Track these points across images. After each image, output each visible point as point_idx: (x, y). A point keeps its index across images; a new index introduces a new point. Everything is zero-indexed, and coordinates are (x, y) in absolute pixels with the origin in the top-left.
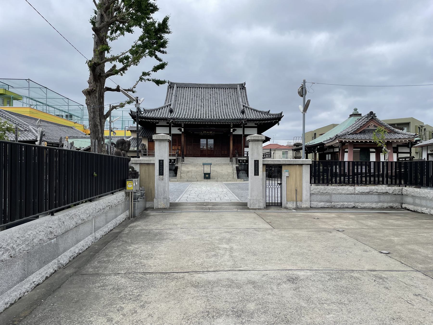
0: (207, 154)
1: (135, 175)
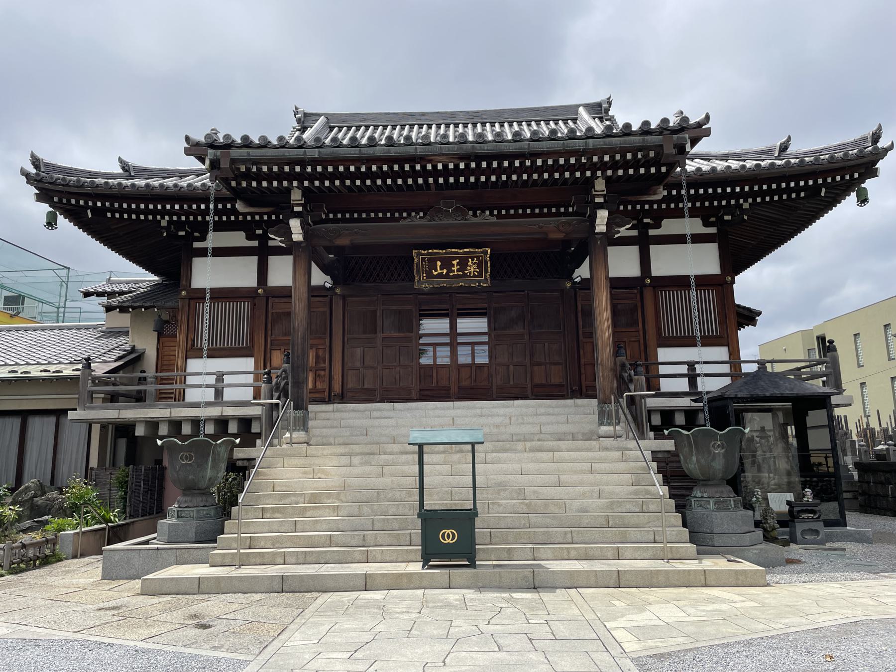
0: (454, 389)
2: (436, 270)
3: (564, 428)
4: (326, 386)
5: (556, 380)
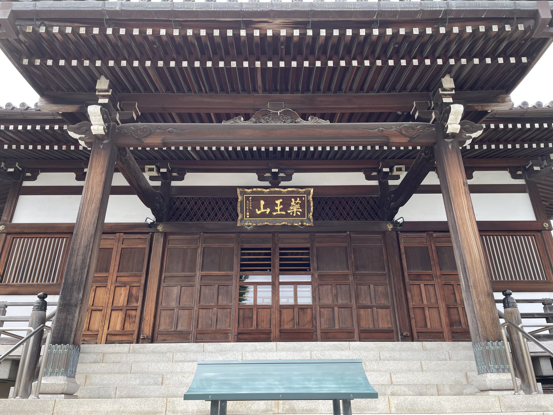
0: (275, 332)
2: (259, 209)
3: (420, 378)
4: (135, 328)
5: (383, 325)
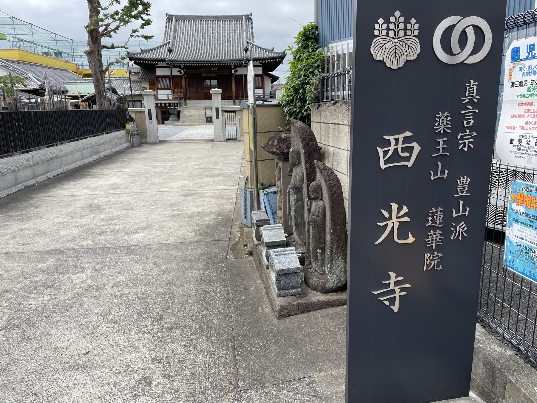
1: (132, 120)
